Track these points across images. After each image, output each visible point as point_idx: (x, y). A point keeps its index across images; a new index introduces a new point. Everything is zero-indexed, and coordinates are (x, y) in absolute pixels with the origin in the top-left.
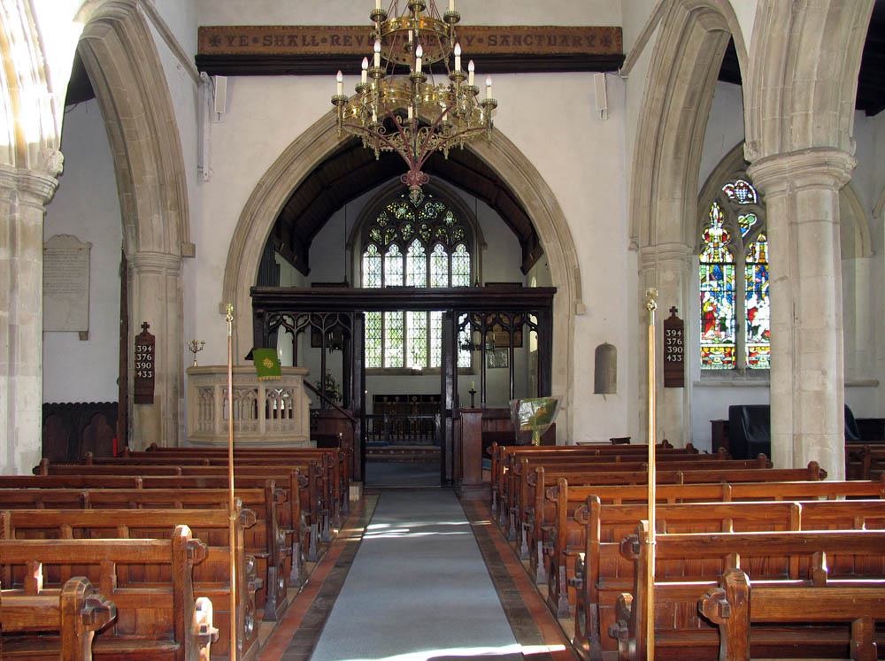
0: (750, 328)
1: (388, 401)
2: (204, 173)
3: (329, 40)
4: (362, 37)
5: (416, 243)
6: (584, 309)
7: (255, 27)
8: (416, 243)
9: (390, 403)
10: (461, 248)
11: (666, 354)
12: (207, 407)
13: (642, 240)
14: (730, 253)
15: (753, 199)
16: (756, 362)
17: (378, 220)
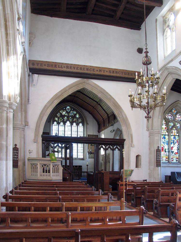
1: (75, 167)
2: (30, 101)
3: (66, 67)
4: (75, 67)
5: (68, 122)
6: (134, 145)
7: (45, 61)
8: (68, 122)
9: (76, 168)
10: (81, 124)
11: (157, 158)
12: (34, 169)
13: (150, 128)
14: (167, 132)
16: (173, 160)
17: (57, 115)
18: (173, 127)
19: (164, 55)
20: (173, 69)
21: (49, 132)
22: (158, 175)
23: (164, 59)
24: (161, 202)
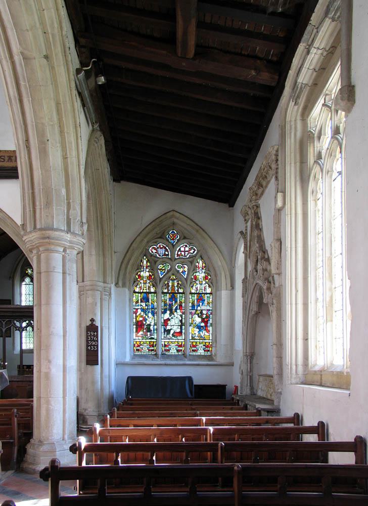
0: (165, 330)
1: (27, 368)
9: (27, 370)
11: (87, 346)
13: (80, 280)
14: (153, 286)
15: (168, 255)
16: (169, 350)
21: (11, 299)
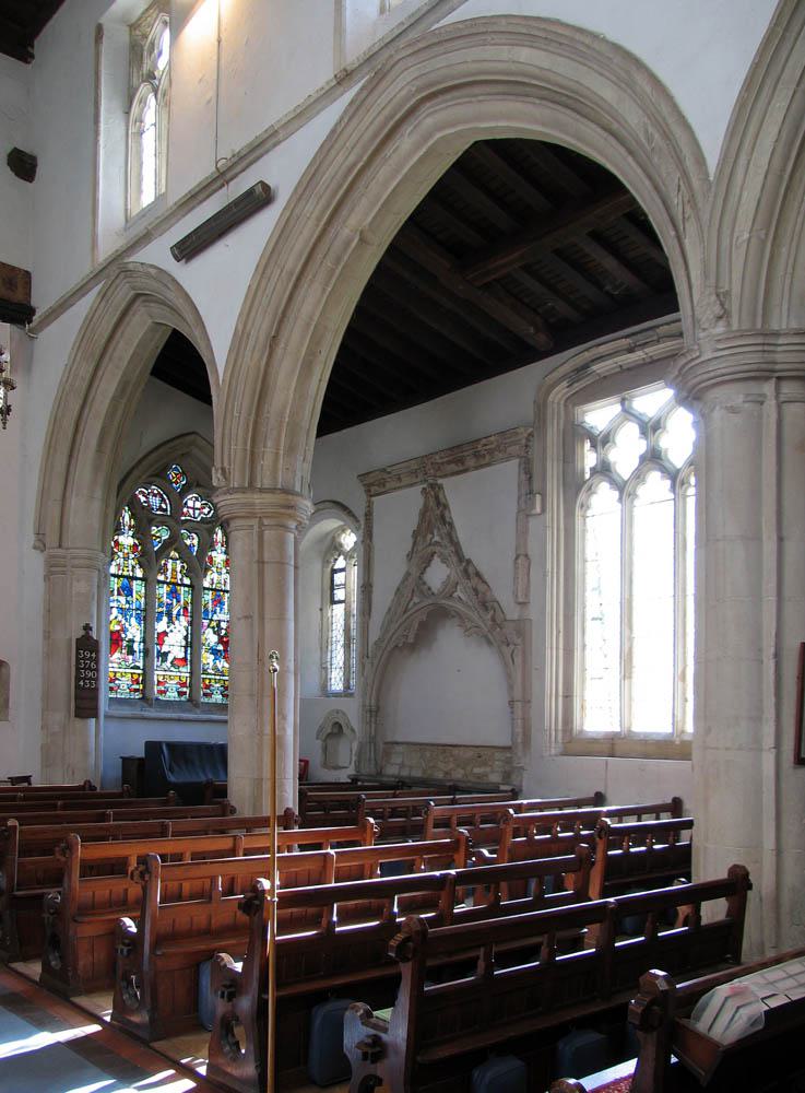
11: (78, 679)
13: (52, 539)
14: (141, 567)
16: (164, 692)
18: (167, 545)
19: (126, 210)
20: (148, 275)
22: (86, 754)
23: (125, 229)
24: (20, 886)
